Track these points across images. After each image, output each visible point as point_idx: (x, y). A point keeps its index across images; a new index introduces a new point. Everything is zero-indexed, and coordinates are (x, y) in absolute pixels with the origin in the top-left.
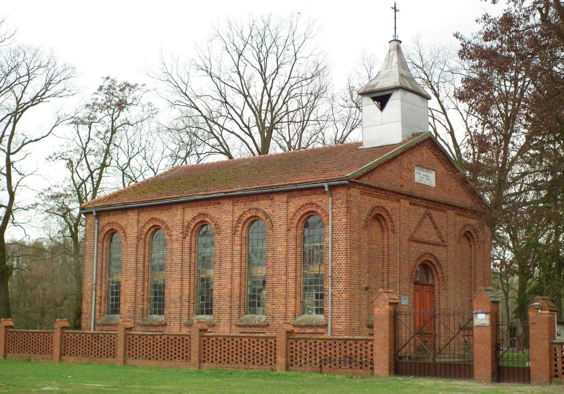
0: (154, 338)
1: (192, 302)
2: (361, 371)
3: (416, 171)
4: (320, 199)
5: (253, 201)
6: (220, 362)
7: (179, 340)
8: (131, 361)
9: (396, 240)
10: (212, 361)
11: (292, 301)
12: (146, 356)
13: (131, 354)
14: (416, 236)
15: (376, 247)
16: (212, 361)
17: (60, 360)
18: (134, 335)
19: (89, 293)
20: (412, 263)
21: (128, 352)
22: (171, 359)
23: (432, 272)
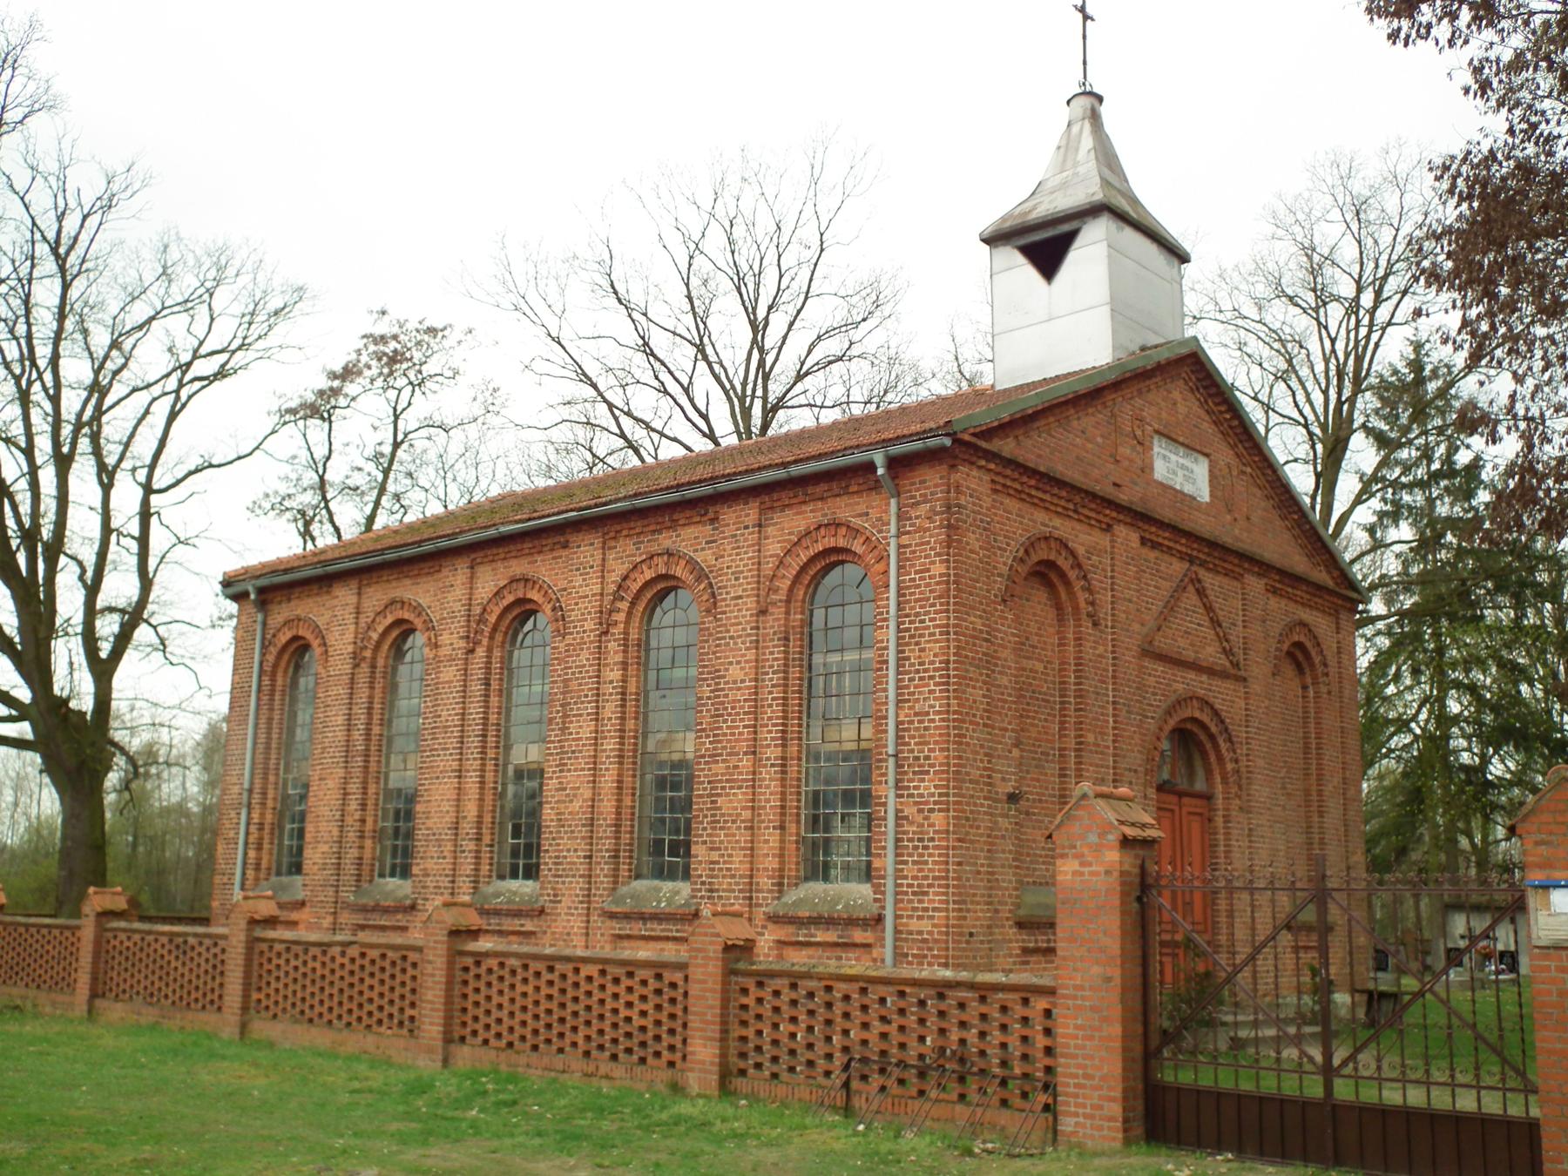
0: (324, 953)
1: (487, 839)
2: (1004, 1117)
3: (1156, 449)
4: (862, 508)
5: (660, 532)
6: (510, 1045)
7: (393, 963)
8: (262, 1028)
9: (1101, 650)
10: (486, 1042)
11: (770, 839)
12: (302, 1012)
13: (264, 1003)
14: (1162, 643)
15: (1040, 667)
16: (486, 1042)
17: (91, 1010)
18: (273, 940)
19: (233, 814)
20: (1151, 724)
21: (255, 996)
22: (369, 1027)
23: (1204, 755)
